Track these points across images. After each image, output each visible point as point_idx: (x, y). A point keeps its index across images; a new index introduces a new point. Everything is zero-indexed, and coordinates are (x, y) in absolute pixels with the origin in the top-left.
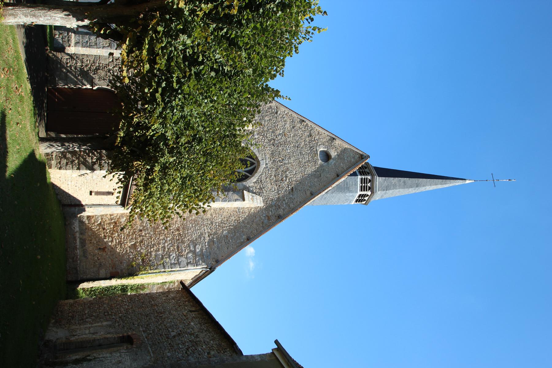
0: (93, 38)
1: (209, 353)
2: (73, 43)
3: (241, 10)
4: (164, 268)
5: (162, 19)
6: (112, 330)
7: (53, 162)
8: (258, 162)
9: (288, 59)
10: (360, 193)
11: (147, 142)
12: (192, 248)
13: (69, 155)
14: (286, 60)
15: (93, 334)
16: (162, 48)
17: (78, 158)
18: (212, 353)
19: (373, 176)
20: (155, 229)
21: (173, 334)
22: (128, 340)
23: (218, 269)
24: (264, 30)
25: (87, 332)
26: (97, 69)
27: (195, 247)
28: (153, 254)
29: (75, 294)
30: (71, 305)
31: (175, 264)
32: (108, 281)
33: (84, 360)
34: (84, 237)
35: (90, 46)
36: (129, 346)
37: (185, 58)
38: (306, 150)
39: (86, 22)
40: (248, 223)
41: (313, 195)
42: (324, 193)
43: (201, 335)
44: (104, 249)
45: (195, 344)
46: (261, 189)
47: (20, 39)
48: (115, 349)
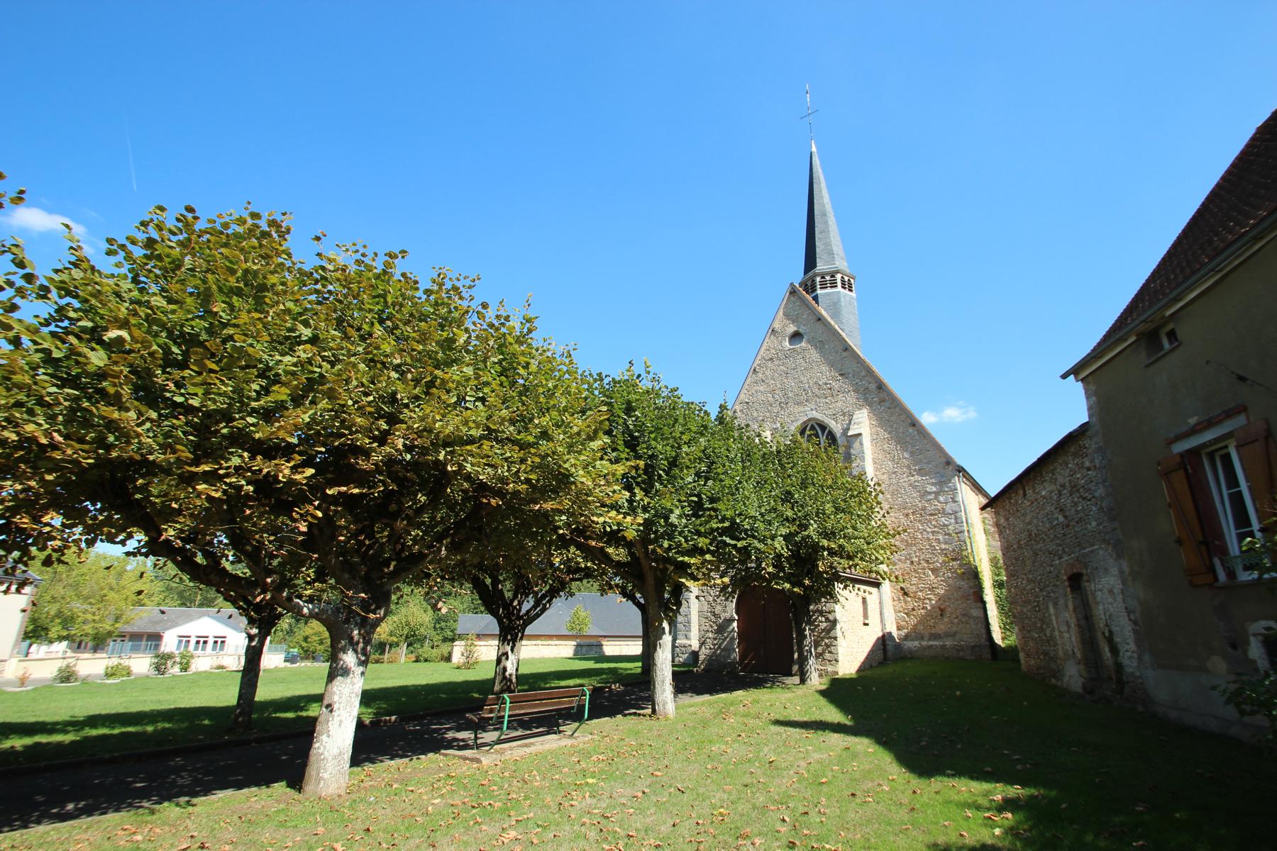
0: (680, 619)
1: (1089, 469)
2: (687, 642)
3: (638, 457)
4: (962, 532)
5: (655, 541)
6: (1061, 602)
7: (830, 669)
8: (809, 420)
9: (685, 399)
10: (839, 288)
11: (795, 555)
12: (932, 497)
13: (820, 649)
14: (686, 401)
15: (1069, 627)
16: (686, 541)
17: (822, 639)
18: (1087, 464)
19: (816, 275)
20: (908, 545)
21: (1061, 519)
22: (1076, 581)
23: (960, 461)
24: (657, 429)
25: (1066, 635)
26: (714, 615)
27: (930, 493)
28: (943, 546)
29: (1011, 652)
30: (1028, 655)
31: (956, 518)
32: (988, 606)
33: (1110, 640)
34: (927, 635)
35: (689, 622)
36: (1085, 578)
37: (696, 515)
38: (790, 362)
39: (665, 625)
40: (891, 427)
41: (847, 348)
42: (843, 334)
43: (1061, 480)
44: (942, 610)
45: (1074, 488)
46: (844, 414)
47: (689, 700)
48: (1090, 597)
